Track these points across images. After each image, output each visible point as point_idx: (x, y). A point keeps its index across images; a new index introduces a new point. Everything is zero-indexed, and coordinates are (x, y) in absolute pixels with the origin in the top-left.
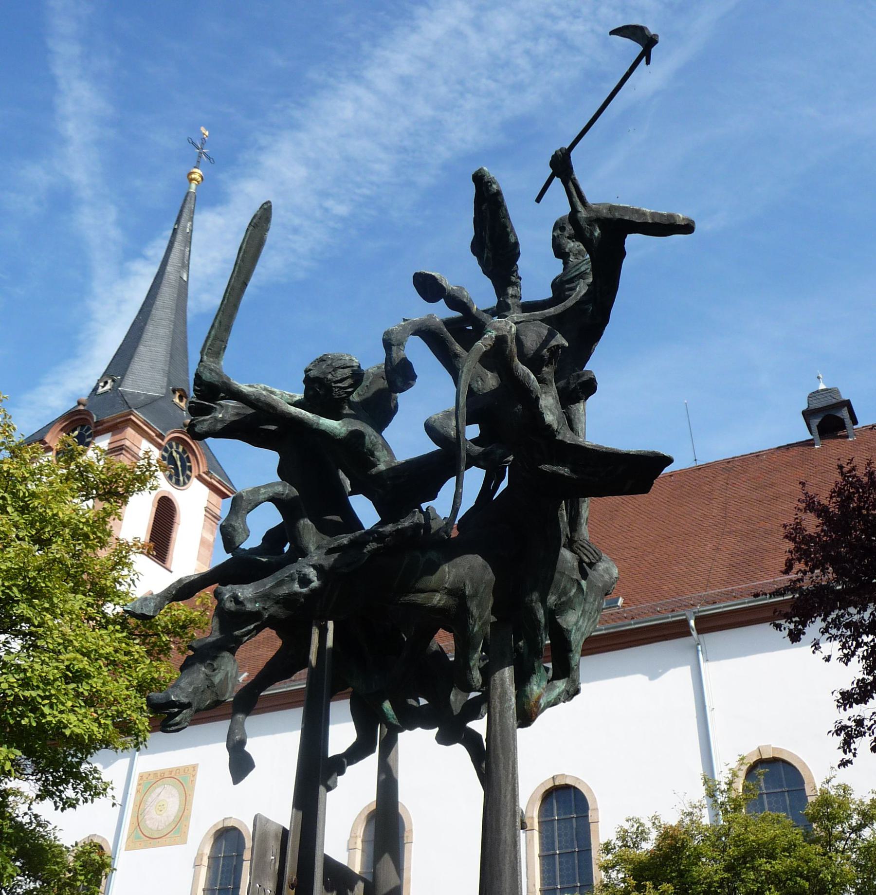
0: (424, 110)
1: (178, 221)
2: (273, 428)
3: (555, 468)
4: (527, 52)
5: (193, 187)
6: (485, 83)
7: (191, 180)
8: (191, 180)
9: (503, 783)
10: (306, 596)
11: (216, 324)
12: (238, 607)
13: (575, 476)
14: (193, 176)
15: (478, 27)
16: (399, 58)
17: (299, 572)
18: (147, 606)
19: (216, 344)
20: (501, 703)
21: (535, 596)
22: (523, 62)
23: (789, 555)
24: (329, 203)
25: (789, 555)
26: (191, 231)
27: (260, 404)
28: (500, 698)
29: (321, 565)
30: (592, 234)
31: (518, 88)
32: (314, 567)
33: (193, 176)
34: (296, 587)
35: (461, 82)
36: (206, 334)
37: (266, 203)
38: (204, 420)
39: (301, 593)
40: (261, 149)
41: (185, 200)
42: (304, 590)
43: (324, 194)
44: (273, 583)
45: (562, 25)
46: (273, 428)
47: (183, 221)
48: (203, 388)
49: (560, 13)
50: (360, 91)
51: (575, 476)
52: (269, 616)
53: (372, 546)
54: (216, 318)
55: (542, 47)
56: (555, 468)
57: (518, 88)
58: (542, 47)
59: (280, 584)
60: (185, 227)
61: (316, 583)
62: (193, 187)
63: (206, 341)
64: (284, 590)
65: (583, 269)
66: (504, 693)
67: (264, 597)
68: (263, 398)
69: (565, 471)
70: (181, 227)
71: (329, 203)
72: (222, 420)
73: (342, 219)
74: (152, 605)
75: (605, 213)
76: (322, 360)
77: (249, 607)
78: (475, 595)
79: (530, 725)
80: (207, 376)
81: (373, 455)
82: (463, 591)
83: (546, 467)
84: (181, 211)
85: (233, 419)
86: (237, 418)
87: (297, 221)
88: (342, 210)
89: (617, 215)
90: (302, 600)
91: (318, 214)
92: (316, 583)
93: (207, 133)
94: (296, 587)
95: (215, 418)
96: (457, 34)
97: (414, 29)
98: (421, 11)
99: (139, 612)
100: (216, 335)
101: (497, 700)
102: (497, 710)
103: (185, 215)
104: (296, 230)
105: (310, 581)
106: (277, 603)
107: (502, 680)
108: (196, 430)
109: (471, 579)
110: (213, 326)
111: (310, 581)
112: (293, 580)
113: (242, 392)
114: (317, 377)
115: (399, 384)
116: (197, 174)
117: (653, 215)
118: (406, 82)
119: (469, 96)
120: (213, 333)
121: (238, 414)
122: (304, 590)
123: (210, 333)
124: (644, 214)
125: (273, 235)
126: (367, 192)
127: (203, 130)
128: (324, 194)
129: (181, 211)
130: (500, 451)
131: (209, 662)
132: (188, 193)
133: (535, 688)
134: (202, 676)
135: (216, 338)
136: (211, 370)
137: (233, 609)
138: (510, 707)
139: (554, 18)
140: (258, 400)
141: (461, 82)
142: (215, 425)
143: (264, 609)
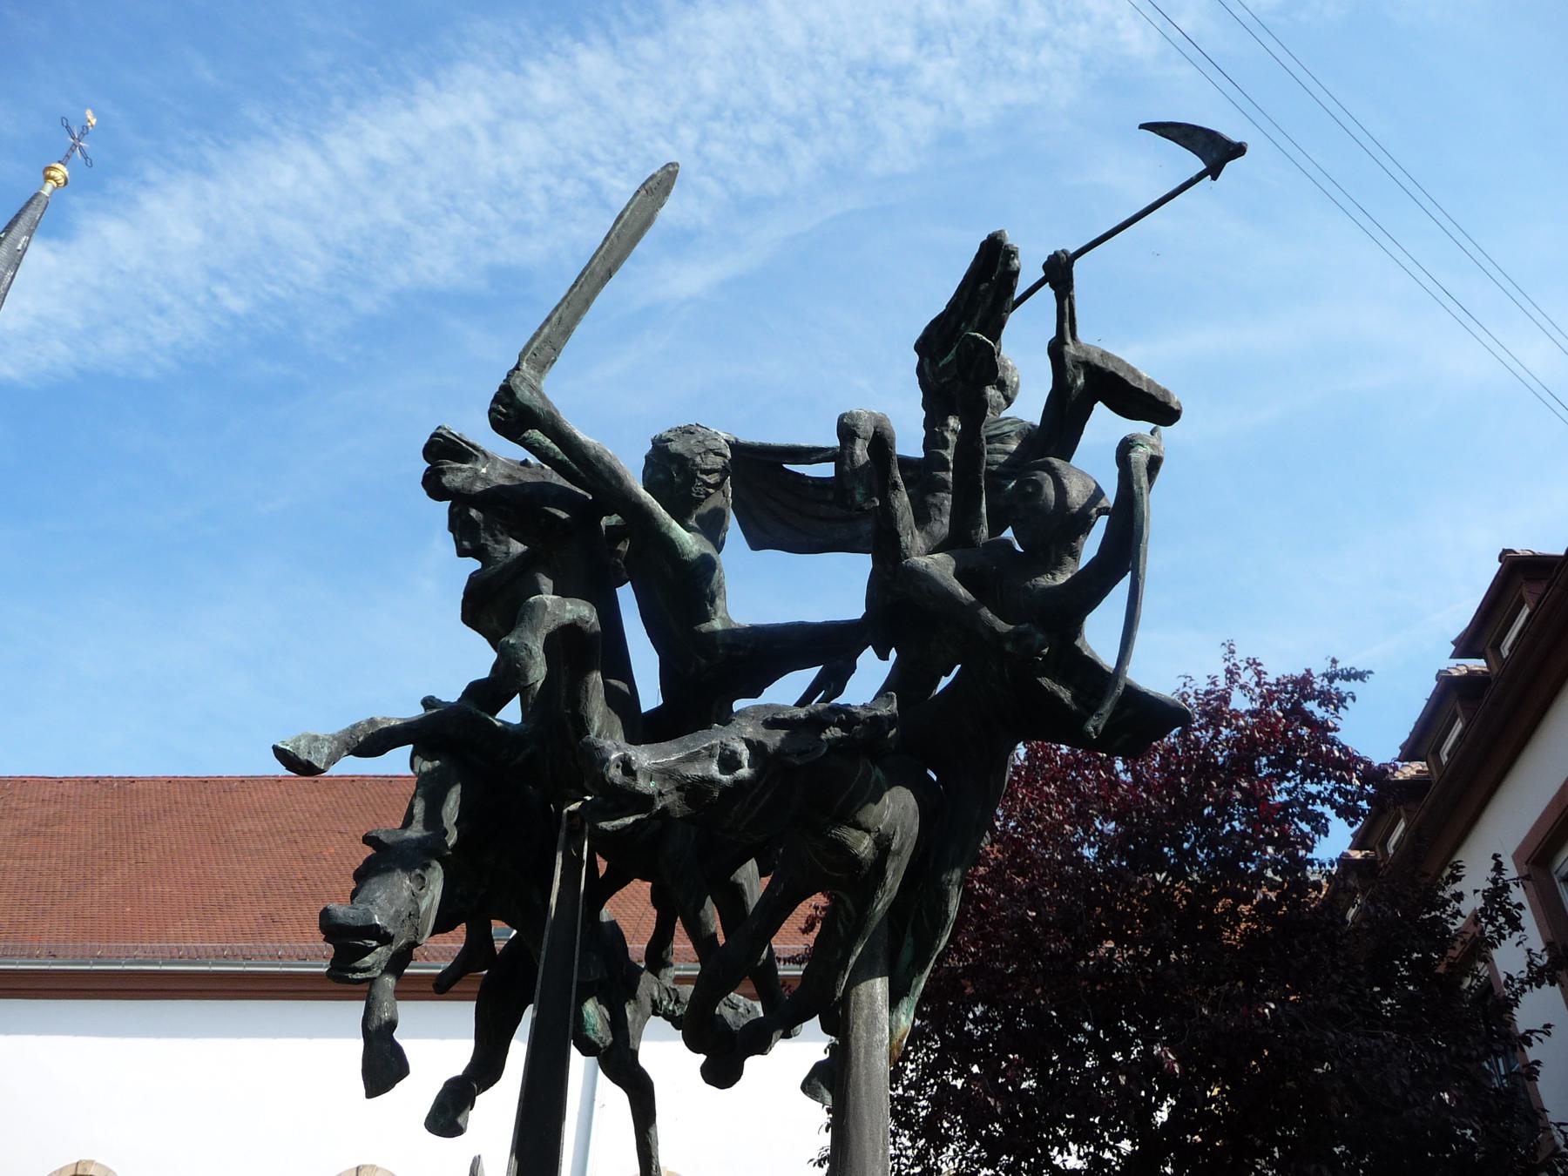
0: (394, 217)
1: (9, 228)
2: (564, 515)
3: (1056, 687)
4: (547, 189)
5: (48, 189)
6: (482, 208)
7: (48, 178)
8: (48, 178)
9: (869, 1157)
10: (725, 790)
11: (554, 319)
12: (627, 779)
13: (1074, 707)
14: (53, 173)
15: (495, 135)
16: (378, 134)
17: (724, 746)
18: (318, 750)
19: (545, 347)
20: (868, 1032)
21: (956, 875)
22: (537, 199)
23: (813, 912)
24: (221, 290)
25: (813, 912)
26: (25, 250)
27: (600, 466)
28: (866, 1024)
29: (760, 743)
30: (1074, 380)
31: (523, 229)
32: (748, 743)
33: (53, 173)
34: (714, 770)
35: (452, 197)
36: (535, 329)
37: (672, 164)
38: (460, 469)
39: (720, 781)
40: (145, 183)
41: (30, 202)
42: (726, 778)
43: (218, 275)
44: (681, 755)
45: (600, 173)
46: (564, 515)
47: (16, 231)
48: (511, 412)
49: (601, 156)
50: (311, 157)
51: (1074, 707)
52: (664, 808)
53: (834, 732)
54: (556, 309)
55: (568, 190)
56: (1056, 687)
57: (523, 229)
58: (568, 190)
59: (692, 758)
60: (18, 241)
61: (745, 772)
62: (48, 189)
63: (533, 339)
64: (695, 771)
65: (1006, 429)
66: (874, 1017)
67: (666, 773)
68: (607, 458)
69: (1065, 695)
70: (9, 239)
71: (221, 290)
72: (485, 479)
73: (234, 317)
74: (326, 750)
75: (1097, 361)
76: (688, 431)
77: (644, 785)
78: (898, 853)
79: (447, 1083)
80: (524, 394)
81: (712, 602)
82: (890, 840)
83: (1046, 682)
84: (18, 216)
85: (502, 482)
86: (507, 483)
87: (167, 299)
88: (237, 304)
89: (1111, 367)
90: (716, 794)
91: (201, 299)
92: (745, 772)
93: (94, 121)
94: (714, 770)
95: (476, 472)
96: (465, 133)
97: (410, 107)
98: (426, 87)
99: (303, 756)
100: (548, 336)
101: (862, 1027)
102: (862, 1043)
103: (23, 224)
104: (161, 311)
105: (739, 765)
106: (678, 789)
107: (872, 998)
108: (444, 480)
109: (903, 826)
110: (548, 320)
111: (739, 765)
112: (711, 756)
113: (576, 437)
114: (681, 455)
115: (858, 498)
116: (61, 172)
117: (1150, 382)
118: (379, 171)
119: (456, 216)
120: (546, 330)
121: (510, 477)
122: (726, 778)
123: (541, 328)
124: (1140, 378)
125: (671, 211)
126: (280, 292)
127: (89, 114)
128: (218, 275)
129: (18, 216)
130: (1040, 636)
131: (418, 871)
132: (37, 194)
133: (903, 1018)
134: (406, 894)
135: (547, 341)
136: (532, 387)
137: (617, 781)
138: (882, 1041)
139: (593, 161)
140: (599, 459)
141: (452, 197)
142: (472, 484)
143: (660, 794)
